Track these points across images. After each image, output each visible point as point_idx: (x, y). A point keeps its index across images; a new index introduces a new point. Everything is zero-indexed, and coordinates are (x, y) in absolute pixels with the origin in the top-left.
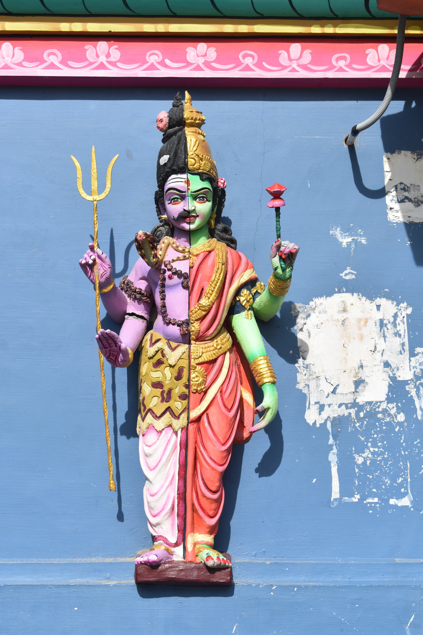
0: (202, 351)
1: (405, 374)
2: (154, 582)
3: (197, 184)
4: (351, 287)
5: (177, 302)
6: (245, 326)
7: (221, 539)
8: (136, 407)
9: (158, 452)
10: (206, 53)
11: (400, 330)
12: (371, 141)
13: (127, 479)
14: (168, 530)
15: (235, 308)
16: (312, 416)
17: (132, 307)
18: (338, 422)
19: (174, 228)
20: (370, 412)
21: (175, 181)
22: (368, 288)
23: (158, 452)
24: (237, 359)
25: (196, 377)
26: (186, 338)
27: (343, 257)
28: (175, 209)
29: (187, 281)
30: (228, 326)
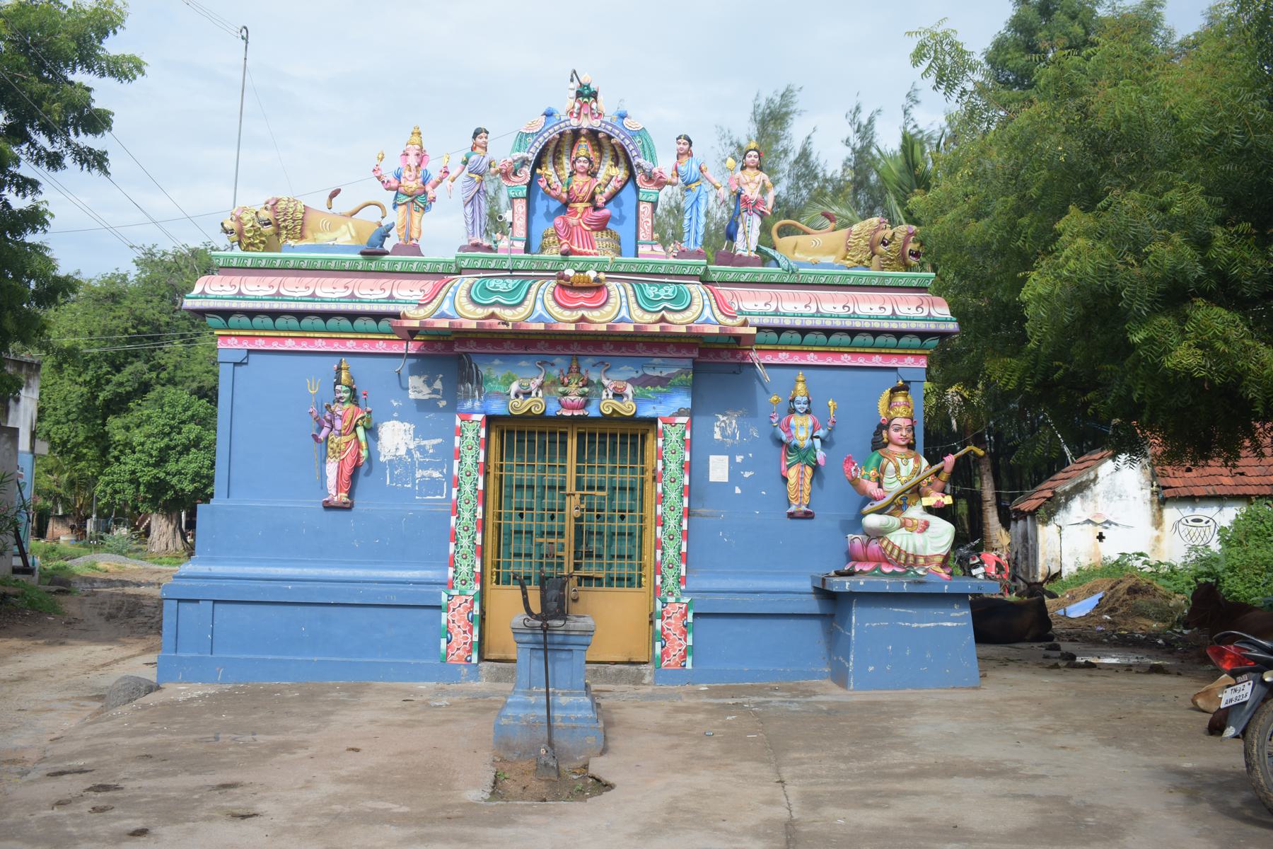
0: (345, 439)
1: (412, 447)
2: (328, 507)
3: (344, 388)
4: (396, 419)
5: (338, 424)
6: (360, 431)
7: (351, 494)
8: (327, 455)
9: (331, 469)
10: (1085, 522)
11: (586, 94)
12: (405, 372)
13: (323, 477)
14: (333, 491)
15: (356, 426)
16: (382, 459)
17: (326, 424)
18: (390, 461)
19: (338, 400)
20: (400, 458)
21: (338, 387)
22: (401, 419)
23: (331, 469)
24: (505, 323)
25: (343, 447)
26: (340, 435)
27: (395, 409)
28: (338, 395)
29: (341, 417)
30: (355, 430)
